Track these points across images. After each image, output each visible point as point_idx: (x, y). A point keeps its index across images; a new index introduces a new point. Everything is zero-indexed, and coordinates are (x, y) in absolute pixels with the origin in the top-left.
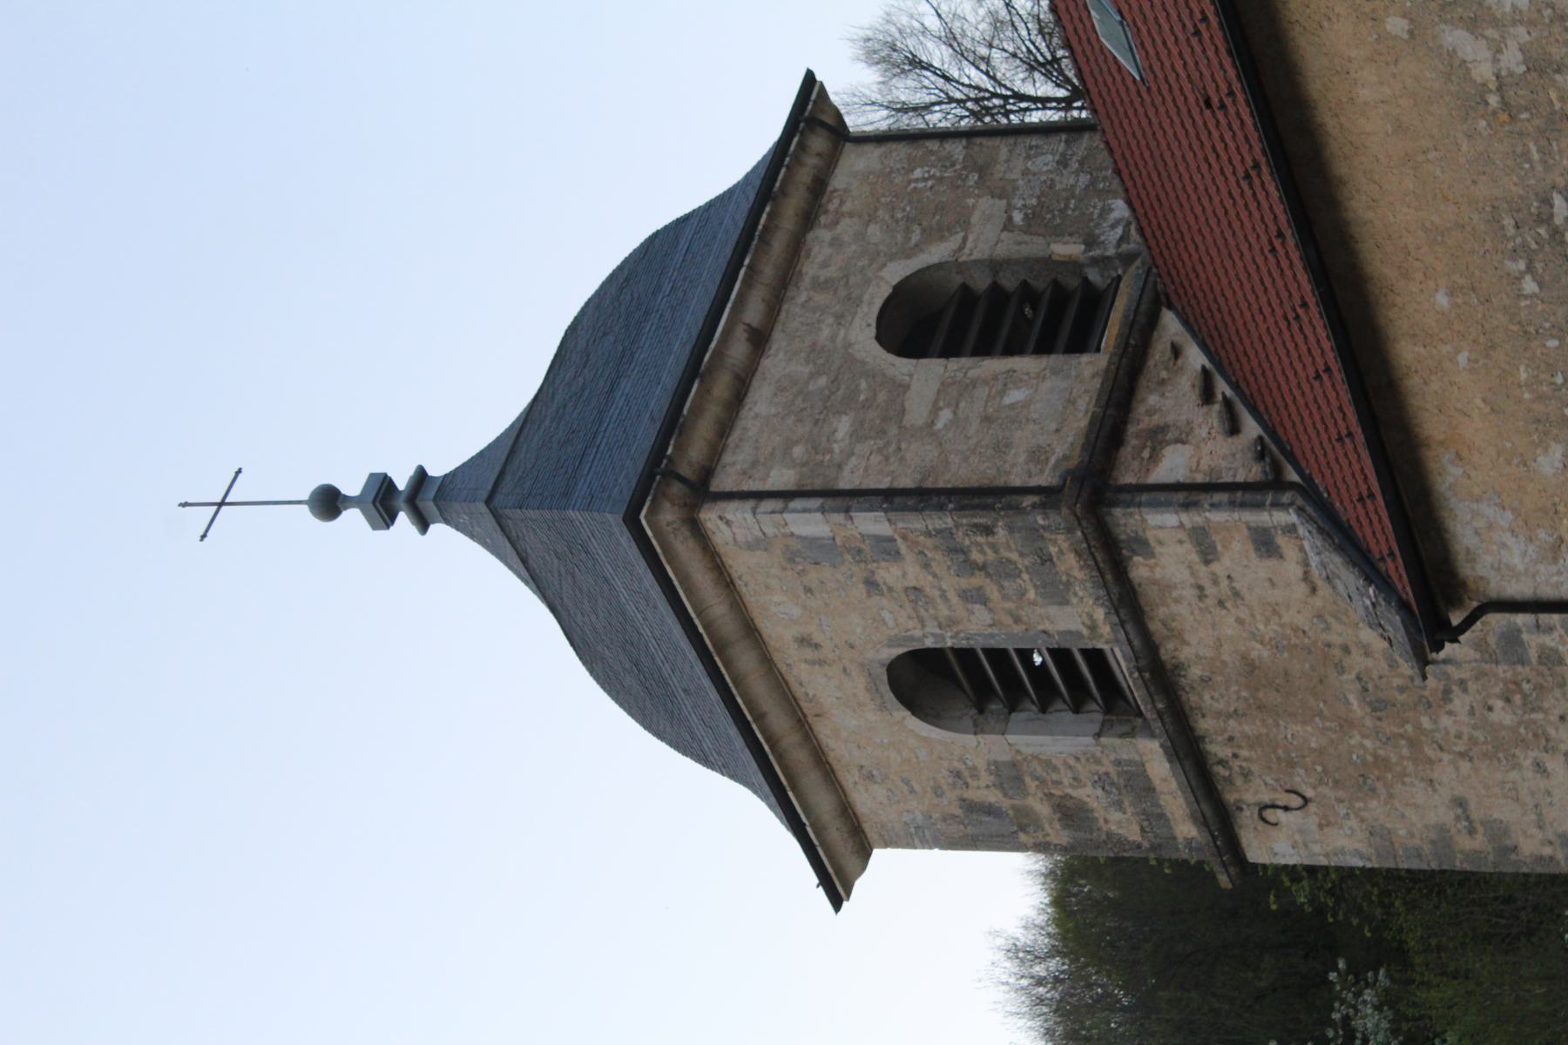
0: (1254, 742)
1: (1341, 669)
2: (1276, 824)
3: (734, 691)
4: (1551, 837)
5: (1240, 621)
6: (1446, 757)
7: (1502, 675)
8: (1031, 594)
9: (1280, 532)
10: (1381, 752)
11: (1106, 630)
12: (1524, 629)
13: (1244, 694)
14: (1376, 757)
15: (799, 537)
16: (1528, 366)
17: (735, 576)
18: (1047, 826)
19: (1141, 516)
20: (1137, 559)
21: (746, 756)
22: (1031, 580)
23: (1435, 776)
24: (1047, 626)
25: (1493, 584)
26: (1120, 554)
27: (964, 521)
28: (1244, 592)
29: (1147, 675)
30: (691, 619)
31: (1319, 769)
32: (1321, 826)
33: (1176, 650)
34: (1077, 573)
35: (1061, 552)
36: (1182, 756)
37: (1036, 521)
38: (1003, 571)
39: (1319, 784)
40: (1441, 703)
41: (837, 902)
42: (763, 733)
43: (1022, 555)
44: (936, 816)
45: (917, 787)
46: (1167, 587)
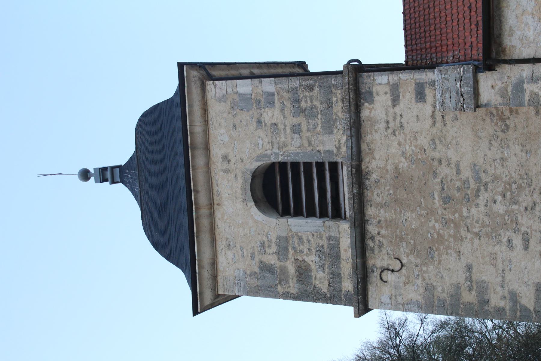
0: (389, 224)
1: (435, 175)
2: (386, 282)
4: (506, 295)
5: (399, 144)
6: (469, 236)
7: (504, 179)
8: (319, 128)
9: (428, 85)
10: (441, 232)
11: (344, 149)
13: (391, 192)
14: (438, 234)
18: (291, 282)
19: (373, 77)
20: (366, 104)
22: (321, 118)
23: (462, 249)
24: (320, 148)
27: (304, 83)
28: (405, 125)
29: (354, 170)
30: (189, 166)
31: (412, 242)
32: (405, 284)
33: (369, 162)
34: (340, 115)
36: (357, 225)
37: (331, 82)
39: (411, 254)
40: (474, 198)
45: (245, 254)
46: (374, 122)
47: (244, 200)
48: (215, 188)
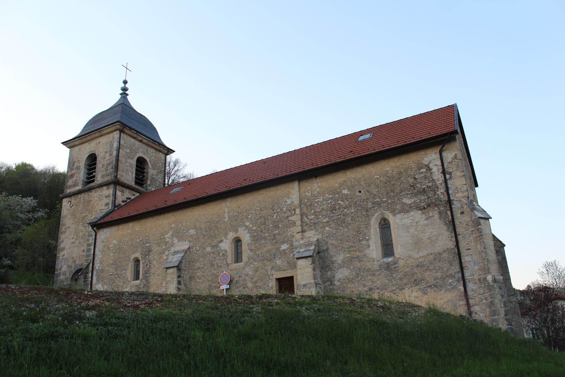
0: (80, 201)
1: (89, 213)
5: (97, 200)
8: (103, 173)
38: (106, 170)
41: (62, 143)
46: (102, 191)
47: (89, 152)
48: (93, 141)
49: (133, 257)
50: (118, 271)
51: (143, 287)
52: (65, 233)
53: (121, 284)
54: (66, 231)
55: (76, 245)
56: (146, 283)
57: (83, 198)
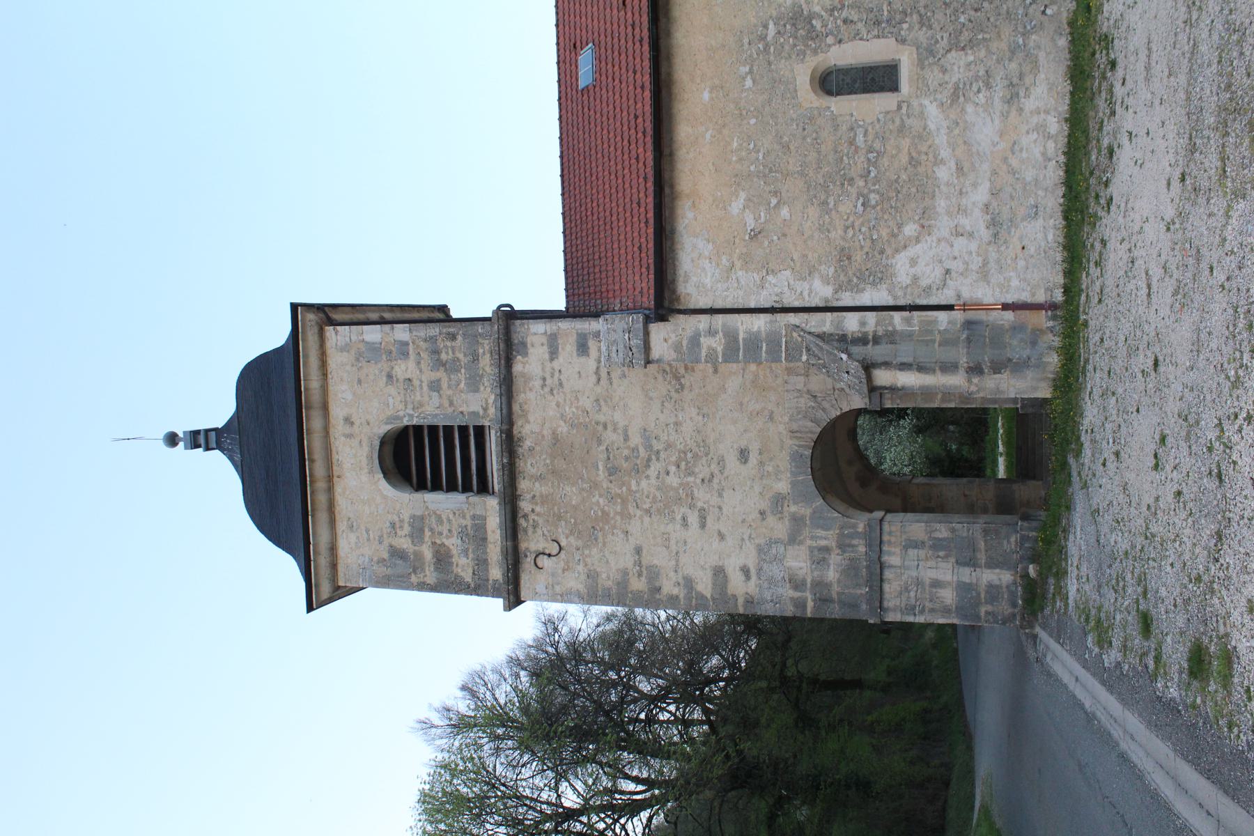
0: (545, 499)
1: (599, 442)
3: (305, 436)
5: (558, 405)
8: (462, 385)
10: (606, 508)
12: (702, 333)
15: (367, 343)
16: (739, 137)
17: (329, 371)
20: (519, 357)
21: (302, 555)
23: (630, 528)
25: (693, 300)
26: (511, 354)
29: (504, 436)
31: (573, 521)
32: (564, 570)
34: (488, 369)
35: (484, 353)
38: (451, 367)
42: (310, 469)
43: (465, 355)
44: (375, 559)
47: (371, 472)
48: (335, 457)
49: (809, 98)
50: (853, 173)
51: (930, 27)
52: (658, 574)
53: (906, 143)
54: (649, 568)
55: (715, 500)
56: (915, 17)
57: (537, 484)
